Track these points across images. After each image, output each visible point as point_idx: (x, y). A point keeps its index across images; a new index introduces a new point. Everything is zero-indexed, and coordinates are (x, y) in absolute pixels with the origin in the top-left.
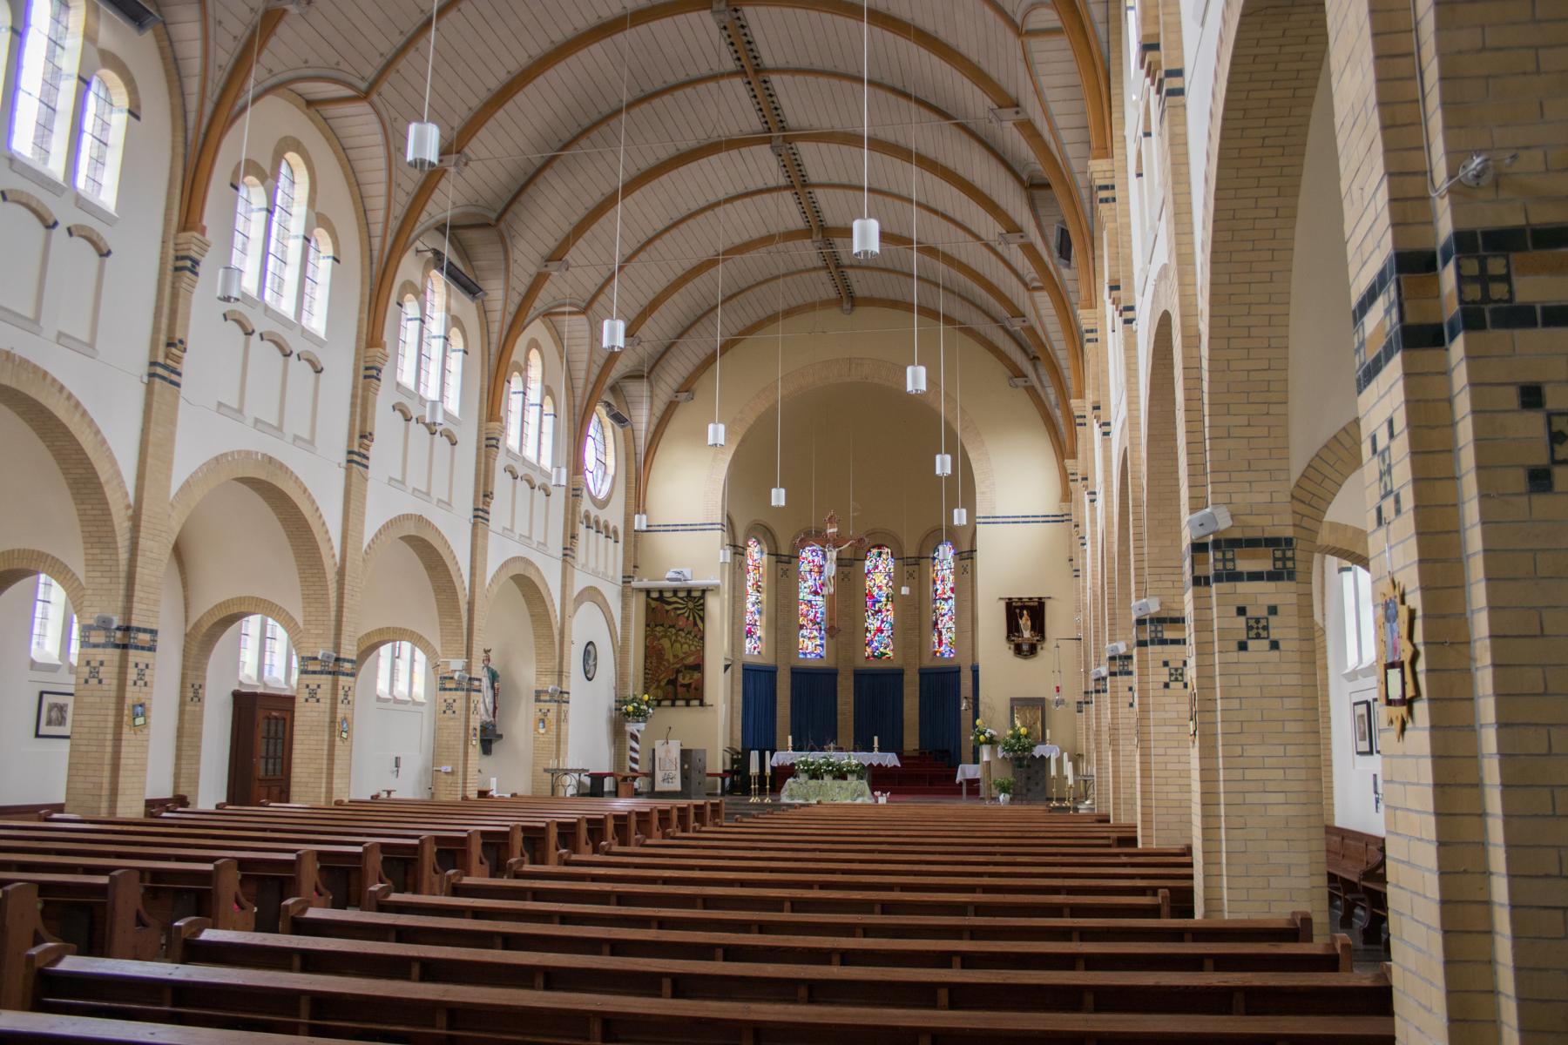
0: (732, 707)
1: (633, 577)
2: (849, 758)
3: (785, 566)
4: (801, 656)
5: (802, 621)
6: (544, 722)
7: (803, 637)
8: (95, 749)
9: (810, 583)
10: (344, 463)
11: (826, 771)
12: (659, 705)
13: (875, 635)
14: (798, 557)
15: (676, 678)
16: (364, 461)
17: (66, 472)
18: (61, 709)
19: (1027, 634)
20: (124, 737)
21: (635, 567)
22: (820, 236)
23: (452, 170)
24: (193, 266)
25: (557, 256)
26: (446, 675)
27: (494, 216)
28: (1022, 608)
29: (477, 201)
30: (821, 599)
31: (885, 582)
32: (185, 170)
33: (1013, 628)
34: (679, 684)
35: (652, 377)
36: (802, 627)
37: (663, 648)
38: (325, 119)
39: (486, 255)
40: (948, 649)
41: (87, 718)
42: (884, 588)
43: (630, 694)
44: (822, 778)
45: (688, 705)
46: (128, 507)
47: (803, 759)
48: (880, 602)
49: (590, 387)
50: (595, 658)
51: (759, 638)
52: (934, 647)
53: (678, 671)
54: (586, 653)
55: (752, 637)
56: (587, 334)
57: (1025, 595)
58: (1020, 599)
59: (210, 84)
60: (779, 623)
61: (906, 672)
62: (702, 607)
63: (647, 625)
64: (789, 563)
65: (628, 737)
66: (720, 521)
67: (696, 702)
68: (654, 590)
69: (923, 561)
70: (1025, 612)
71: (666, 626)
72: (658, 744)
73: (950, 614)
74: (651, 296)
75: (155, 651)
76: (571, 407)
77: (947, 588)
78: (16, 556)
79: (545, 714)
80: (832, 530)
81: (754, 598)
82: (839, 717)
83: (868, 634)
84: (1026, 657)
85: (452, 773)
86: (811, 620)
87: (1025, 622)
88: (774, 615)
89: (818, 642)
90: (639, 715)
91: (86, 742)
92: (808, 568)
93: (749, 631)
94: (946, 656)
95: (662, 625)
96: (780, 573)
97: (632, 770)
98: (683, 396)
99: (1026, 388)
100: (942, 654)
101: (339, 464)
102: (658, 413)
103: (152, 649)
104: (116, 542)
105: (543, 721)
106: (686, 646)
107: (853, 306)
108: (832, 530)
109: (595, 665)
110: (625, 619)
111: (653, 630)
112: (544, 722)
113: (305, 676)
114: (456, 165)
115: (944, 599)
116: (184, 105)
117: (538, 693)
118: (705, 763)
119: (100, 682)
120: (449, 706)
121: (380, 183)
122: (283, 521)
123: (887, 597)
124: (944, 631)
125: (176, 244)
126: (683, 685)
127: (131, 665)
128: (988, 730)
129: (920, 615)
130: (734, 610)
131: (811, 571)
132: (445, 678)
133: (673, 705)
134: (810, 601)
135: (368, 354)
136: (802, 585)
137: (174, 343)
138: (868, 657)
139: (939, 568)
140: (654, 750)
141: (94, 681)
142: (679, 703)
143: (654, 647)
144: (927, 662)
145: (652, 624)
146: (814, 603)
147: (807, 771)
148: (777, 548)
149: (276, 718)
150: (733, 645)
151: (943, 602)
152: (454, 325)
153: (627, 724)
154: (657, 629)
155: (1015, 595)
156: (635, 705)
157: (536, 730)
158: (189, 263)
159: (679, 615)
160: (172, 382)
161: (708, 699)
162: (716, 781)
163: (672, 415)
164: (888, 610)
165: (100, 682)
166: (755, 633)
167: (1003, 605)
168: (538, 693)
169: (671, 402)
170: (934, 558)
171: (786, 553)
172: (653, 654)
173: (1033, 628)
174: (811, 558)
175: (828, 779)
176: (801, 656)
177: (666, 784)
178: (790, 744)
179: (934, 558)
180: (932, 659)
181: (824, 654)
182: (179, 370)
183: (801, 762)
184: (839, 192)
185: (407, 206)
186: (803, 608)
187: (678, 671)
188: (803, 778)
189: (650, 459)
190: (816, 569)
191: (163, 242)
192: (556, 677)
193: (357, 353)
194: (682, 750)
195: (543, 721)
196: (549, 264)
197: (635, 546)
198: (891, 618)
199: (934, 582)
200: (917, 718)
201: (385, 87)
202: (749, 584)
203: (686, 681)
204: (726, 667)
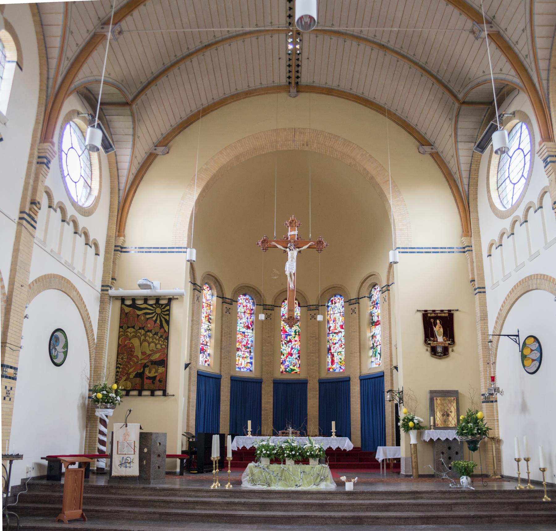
0: (189, 402)
1: (111, 287)
3: (228, 306)
4: (237, 369)
5: (238, 345)
9: (244, 320)
12: (127, 394)
13: (287, 357)
14: (237, 302)
19: (440, 339)
21: (113, 279)
28: (436, 318)
30: (251, 331)
33: (429, 334)
34: (145, 377)
36: (238, 349)
37: (133, 347)
40: (338, 366)
43: (103, 382)
44: (284, 463)
45: (152, 395)
47: (264, 443)
48: (290, 335)
50: (66, 346)
51: (209, 354)
52: (328, 365)
53: (145, 366)
57: (438, 308)
58: (434, 311)
60: (224, 344)
61: (309, 382)
62: (168, 313)
63: (121, 327)
64: (231, 304)
67: (160, 393)
68: (128, 298)
70: (438, 321)
73: (340, 342)
75: (16, 380)
76: (45, 79)
77: (338, 326)
80: (293, 233)
81: (206, 326)
82: (263, 412)
83: (282, 357)
84: (440, 357)
86: (244, 346)
87: (438, 329)
88: (220, 338)
89: (249, 360)
90: (108, 401)
92: (243, 310)
94: (337, 371)
95: (133, 327)
96: (225, 310)
98: (160, 149)
99: (432, 155)
100: (334, 370)
103: (14, 379)
106: (152, 345)
107: (298, 92)
108: (293, 233)
110: (102, 322)
111: (125, 331)
115: (335, 333)
118: (165, 446)
124: (335, 354)
126: (149, 378)
128: (416, 418)
129: (319, 343)
130: (192, 330)
131: (245, 312)
133: (140, 395)
134: (244, 333)
136: (239, 321)
138: (282, 372)
139: (332, 312)
140: (113, 433)
142: (145, 393)
143: (125, 346)
144: (324, 375)
145: (125, 326)
147: (269, 456)
148: (222, 291)
150: (191, 355)
151: (335, 335)
153: (97, 410)
154: (129, 330)
155: (430, 308)
156: (105, 392)
158: (45, 161)
159: (148, 319)
161: (170, 391)
162: (176, 461)
163: (150, 164)
164: (296, 341)
167: (420, 316)
169: (151, 154)
170: (328, 306)
171: (230, 298)
173: (445, 334)
174: (245, 304)
175: (290, 463)
176: (237, 369)
177: (123, 469)
179: (328, 306)
180: (328, 373)
181: (253, 368)
183: (263, 446)
186: (239, 337)
187: (145, 366)
188: (265, 462)
190: (248, 312)
194: (141, 434)
199: (328, 322)
200: (317, 413)
202: (204, 315)
203: (152, 375)
204: (187, 366)
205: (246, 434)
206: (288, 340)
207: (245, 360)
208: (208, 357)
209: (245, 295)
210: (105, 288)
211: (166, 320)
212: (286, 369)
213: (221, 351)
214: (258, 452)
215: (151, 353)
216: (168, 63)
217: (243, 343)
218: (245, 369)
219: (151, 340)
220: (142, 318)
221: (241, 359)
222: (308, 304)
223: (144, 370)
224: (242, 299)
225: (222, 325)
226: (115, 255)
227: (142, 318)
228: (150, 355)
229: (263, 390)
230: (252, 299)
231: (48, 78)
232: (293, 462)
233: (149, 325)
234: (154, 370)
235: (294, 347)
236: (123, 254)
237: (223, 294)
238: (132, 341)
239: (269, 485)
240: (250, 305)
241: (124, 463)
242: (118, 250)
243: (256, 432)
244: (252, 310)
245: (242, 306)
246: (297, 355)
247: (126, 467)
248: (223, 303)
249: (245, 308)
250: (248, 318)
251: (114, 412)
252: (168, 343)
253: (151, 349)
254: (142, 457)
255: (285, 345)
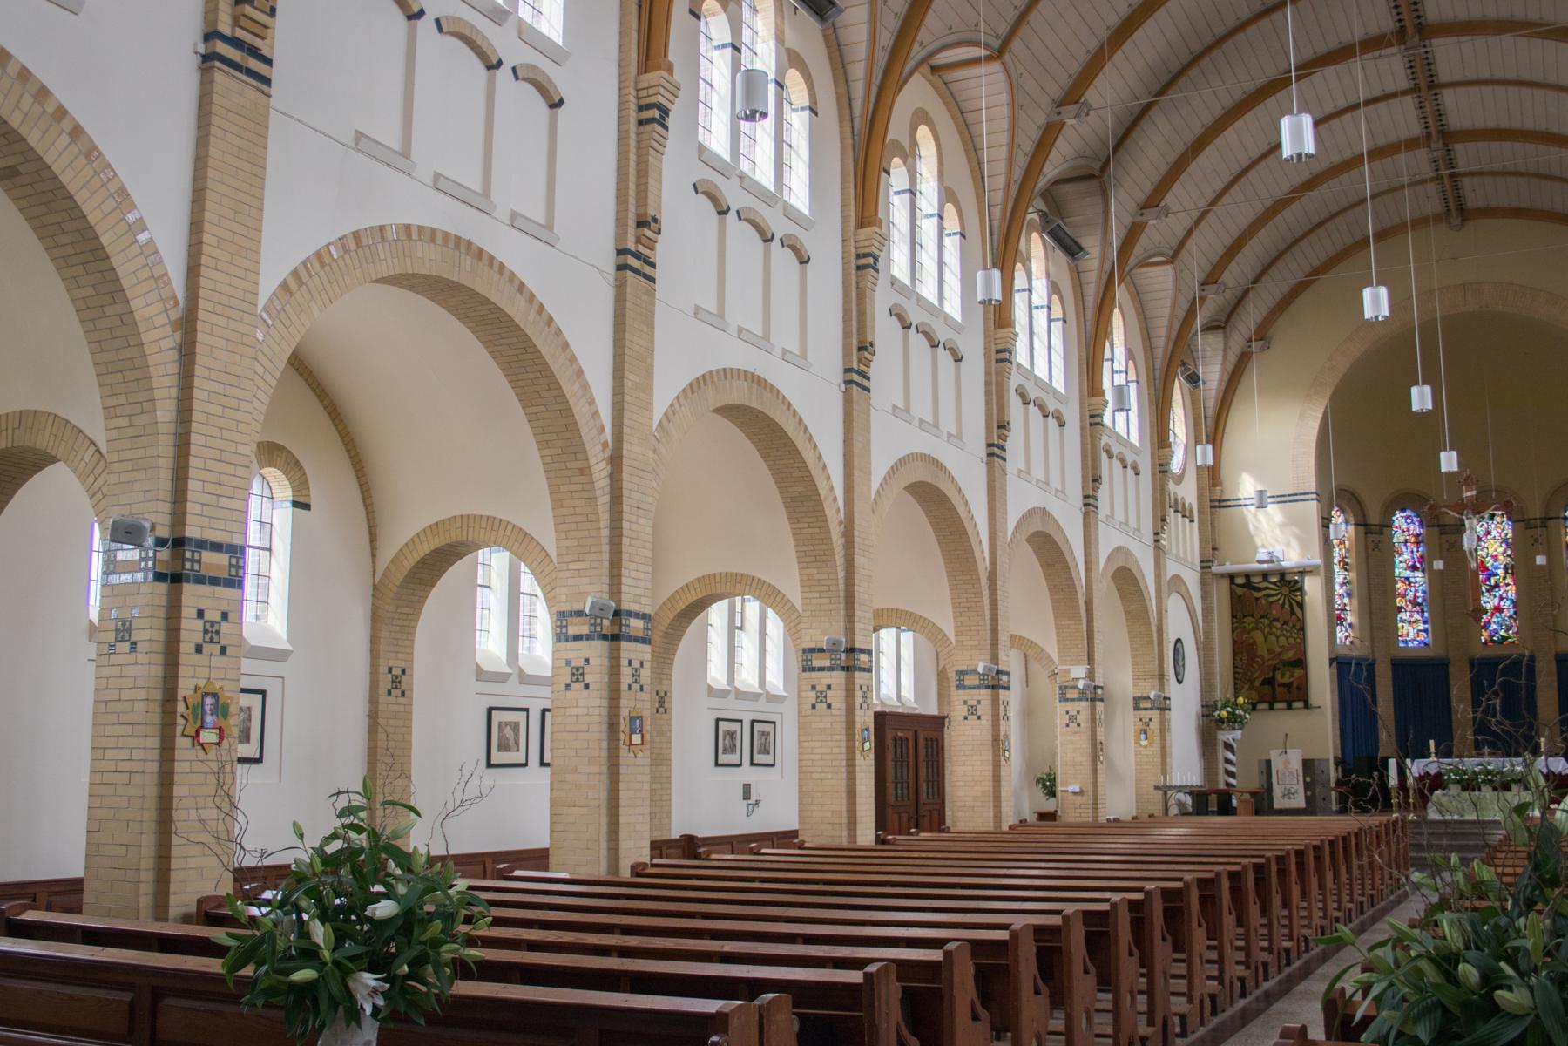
1: (1212, 561)
2: (1513, 765)
5: (1399, 602)
6: (1145, 733)
7: (1403, 621)
8: (830, 776)
10: (984, 455)
11: (1484, 781)
12: (1254, 709)
13: (1492, 615)
14: (1390, 527)
15: (1274, 677)
16: (647, 269)
17: (783, 491)
18: (732, 735)
20: (622, 761)
21: (1214, 549)
22: (1441, 142)
23: (1070, 122)
24: (875, 263)
25: (1152, 202)
26: (1067, 684)
27: (1098, 166)
29: (1084, 152)
31: (1501, 550)
32: (855, 161)
35: (1228, 329)
36: (1400, 609)
37: (1255, 643)
38: (945, 83)
39: (1082, 208)
41: (818, 744)
42: (1501, 558)
44: (1479, 790)
45: (1289, 707)
46: (841, 523)
49: (1171, 345)
50: (1183, 658)
51: (1350, 625)
53: (1275, 669)
54: (1176, 651)
55: (1342, 624)
56: (1170, 285)
59: (875, 66)
63: (1233, 616)
64: (1382, 533)
65: (1221, 747)
66: (1314, 490)
67: (1299, 704)
68: (1239, 574)
69: (1552, 523)
71: (1257, 615)
72: (1274, 756)
74: (1236, 234)
76: (1151, 370)
78: (718, 580)
79: (1147, 724)
80: (1469, 494)
85: (1081, 793)
86: (1410, 601)
89: (1421, 627)
90: (1234, 721)
91: (819, 769)
92: (1402, 539)
93: (1339, 618)
95: (1252, 616)
96: (1371, 546)
97: (1228, 784)
101: (982, 459)
102: (1230, 367)
104: (835, 561)
105: (1145, 732)
106: (1282, 639)
109: (1184, 665)
110: (1207, 611)
111: (1241, 622)
112: (1145, 733)
113: (807, 674)
114: (1077, 116)
116: (849, 92)
117: (1137, 700)
119: (829, 706)
120: (821, 697)
121: (1001, 145)
122: (936, 527)
123: (1506, 568)
125: (856, 242)
127: (188, 612)
131: (1406, 542)
132: (1066, 687)
133: (1272, 708)
134: (1407, 578)
135: (999, 336)
136: (1398, 559)
137: (865, 347)
138: (1485, 643)
141: (821, 706)
142: (1278, 705)
143: (1244, 642)
145: (1239, 614)
146: (1412, 580)
147: (1459, 782)
148: (1364, 516)
149: (901, 738)
152: (1054, 293)
154: (1246, 620)
156: (1229, 709)
157: (1137, 742)
158: (871, 260)
159: (1272, 602)
160: (646, 277)
161: (1314, 701)
164: (1507, 585)
165: (829, 706)
166: (1345, 620)
168: (1137, 700)
172: (1242, 649)
175: (1487, 791)
176: (1402, 645)
177: (1286, 800)
178: (1433, 749)
181: (1429, 640)
182: (265, 52)
183: (1451, 770)
184: (1473, 90)
185: (1024, 169)
187: (1275, 669)
188: (1454, 789)
189: (1222, 422)
191: (843, 241)
192: (1157, 681)
193: (987, 336)
195: (1145, 732)
196: (1144, 211)
197: (1212, 525)
198: (1511, 592)
201: (1016, 44)
202: (1336, 561)
203: (1286, 680)
205: (1429, 756)
206: (1493, 583)
207: (1415, 625)
208: (1350, 631)
209: (1403, 510)
210: (1206, 564)
211: (1297, 602)
212: (1492, 636)
213: (1371, 618)
214: (1446, 777)
215: (1280, 650)
216: (1197, 47)
217: (1408, 597)
218: (1415, 643)
219: (1279, 632)
220: (1263, 602)
221: (1406, 625)
222: (1526, 517)
223: (1274, 675)
224: (1399, 519)
225: (1368, 573)
226: (1212, 514)
227: (1263, 602)
228: (1280, 654)
229: (1451, 676)
230: (1418, 516)
231: (1154, 369)
232: (1490, 789)
233: (1274, 612)
234: (1287, 674)
235: (1504, 595)
236: (1222, 509)
237: (1365, 520)
238: (1252, 634)
239: (1462, 816)
240: (1415, 528)
241: (1288, 794)
242: (1215, 507)
243: (1446, 753)
244: (1418, 535)
245: (1400, 531)
246: (1512, 611)
247: (1290, 798)
248: (1366, 533)
249: (1406, 533)
250: (1412, 552)
251: (1242, 735)
252: (1304, 635)
253: (1281, 644)
254: (1307, 787)
255: (1486, 594)
